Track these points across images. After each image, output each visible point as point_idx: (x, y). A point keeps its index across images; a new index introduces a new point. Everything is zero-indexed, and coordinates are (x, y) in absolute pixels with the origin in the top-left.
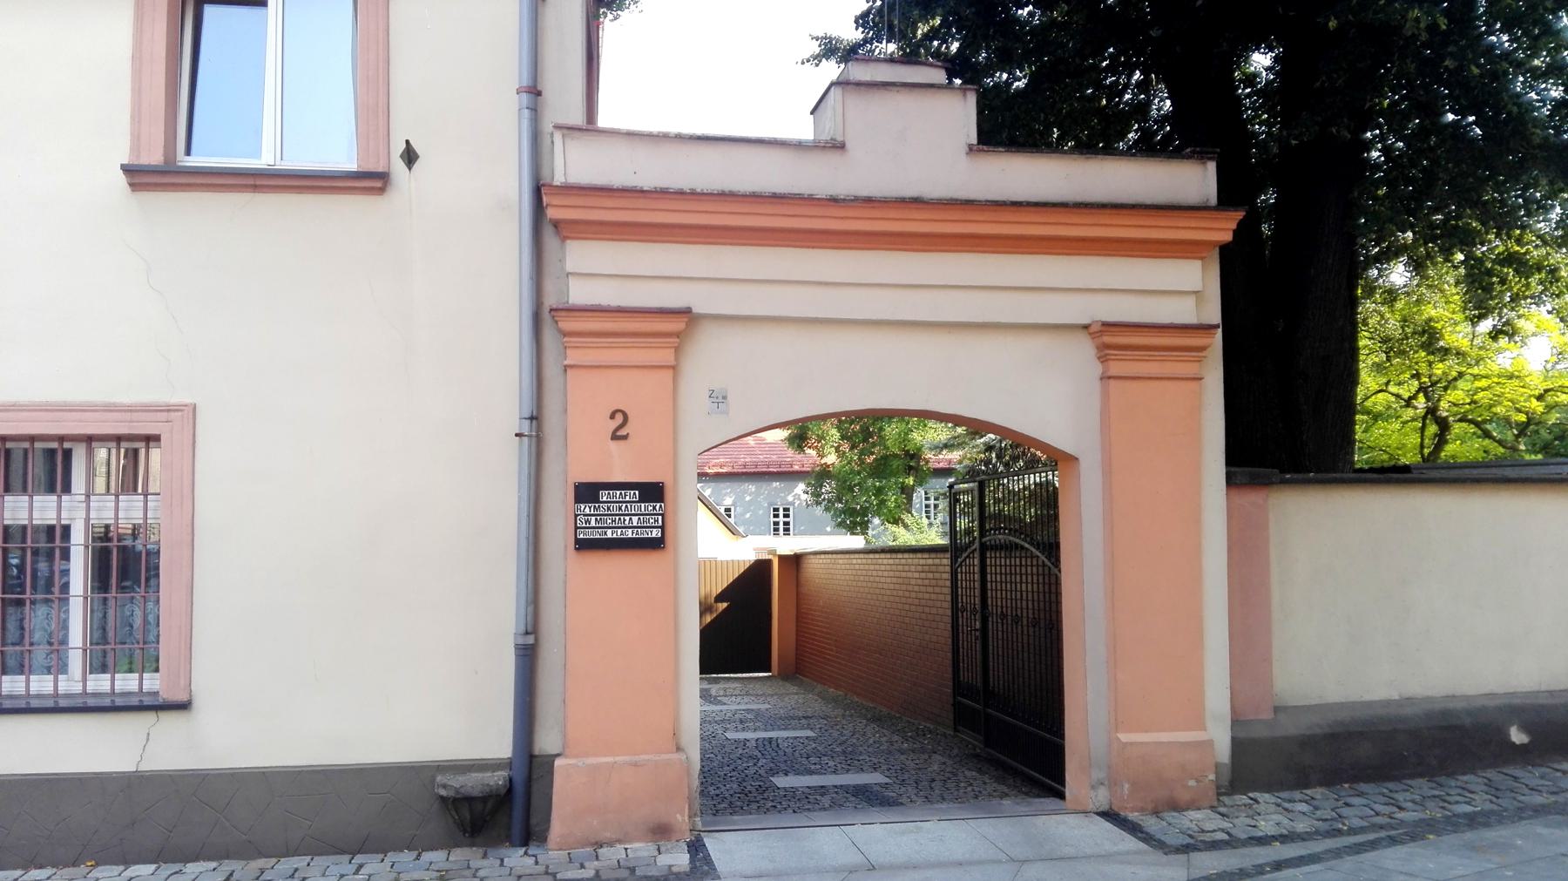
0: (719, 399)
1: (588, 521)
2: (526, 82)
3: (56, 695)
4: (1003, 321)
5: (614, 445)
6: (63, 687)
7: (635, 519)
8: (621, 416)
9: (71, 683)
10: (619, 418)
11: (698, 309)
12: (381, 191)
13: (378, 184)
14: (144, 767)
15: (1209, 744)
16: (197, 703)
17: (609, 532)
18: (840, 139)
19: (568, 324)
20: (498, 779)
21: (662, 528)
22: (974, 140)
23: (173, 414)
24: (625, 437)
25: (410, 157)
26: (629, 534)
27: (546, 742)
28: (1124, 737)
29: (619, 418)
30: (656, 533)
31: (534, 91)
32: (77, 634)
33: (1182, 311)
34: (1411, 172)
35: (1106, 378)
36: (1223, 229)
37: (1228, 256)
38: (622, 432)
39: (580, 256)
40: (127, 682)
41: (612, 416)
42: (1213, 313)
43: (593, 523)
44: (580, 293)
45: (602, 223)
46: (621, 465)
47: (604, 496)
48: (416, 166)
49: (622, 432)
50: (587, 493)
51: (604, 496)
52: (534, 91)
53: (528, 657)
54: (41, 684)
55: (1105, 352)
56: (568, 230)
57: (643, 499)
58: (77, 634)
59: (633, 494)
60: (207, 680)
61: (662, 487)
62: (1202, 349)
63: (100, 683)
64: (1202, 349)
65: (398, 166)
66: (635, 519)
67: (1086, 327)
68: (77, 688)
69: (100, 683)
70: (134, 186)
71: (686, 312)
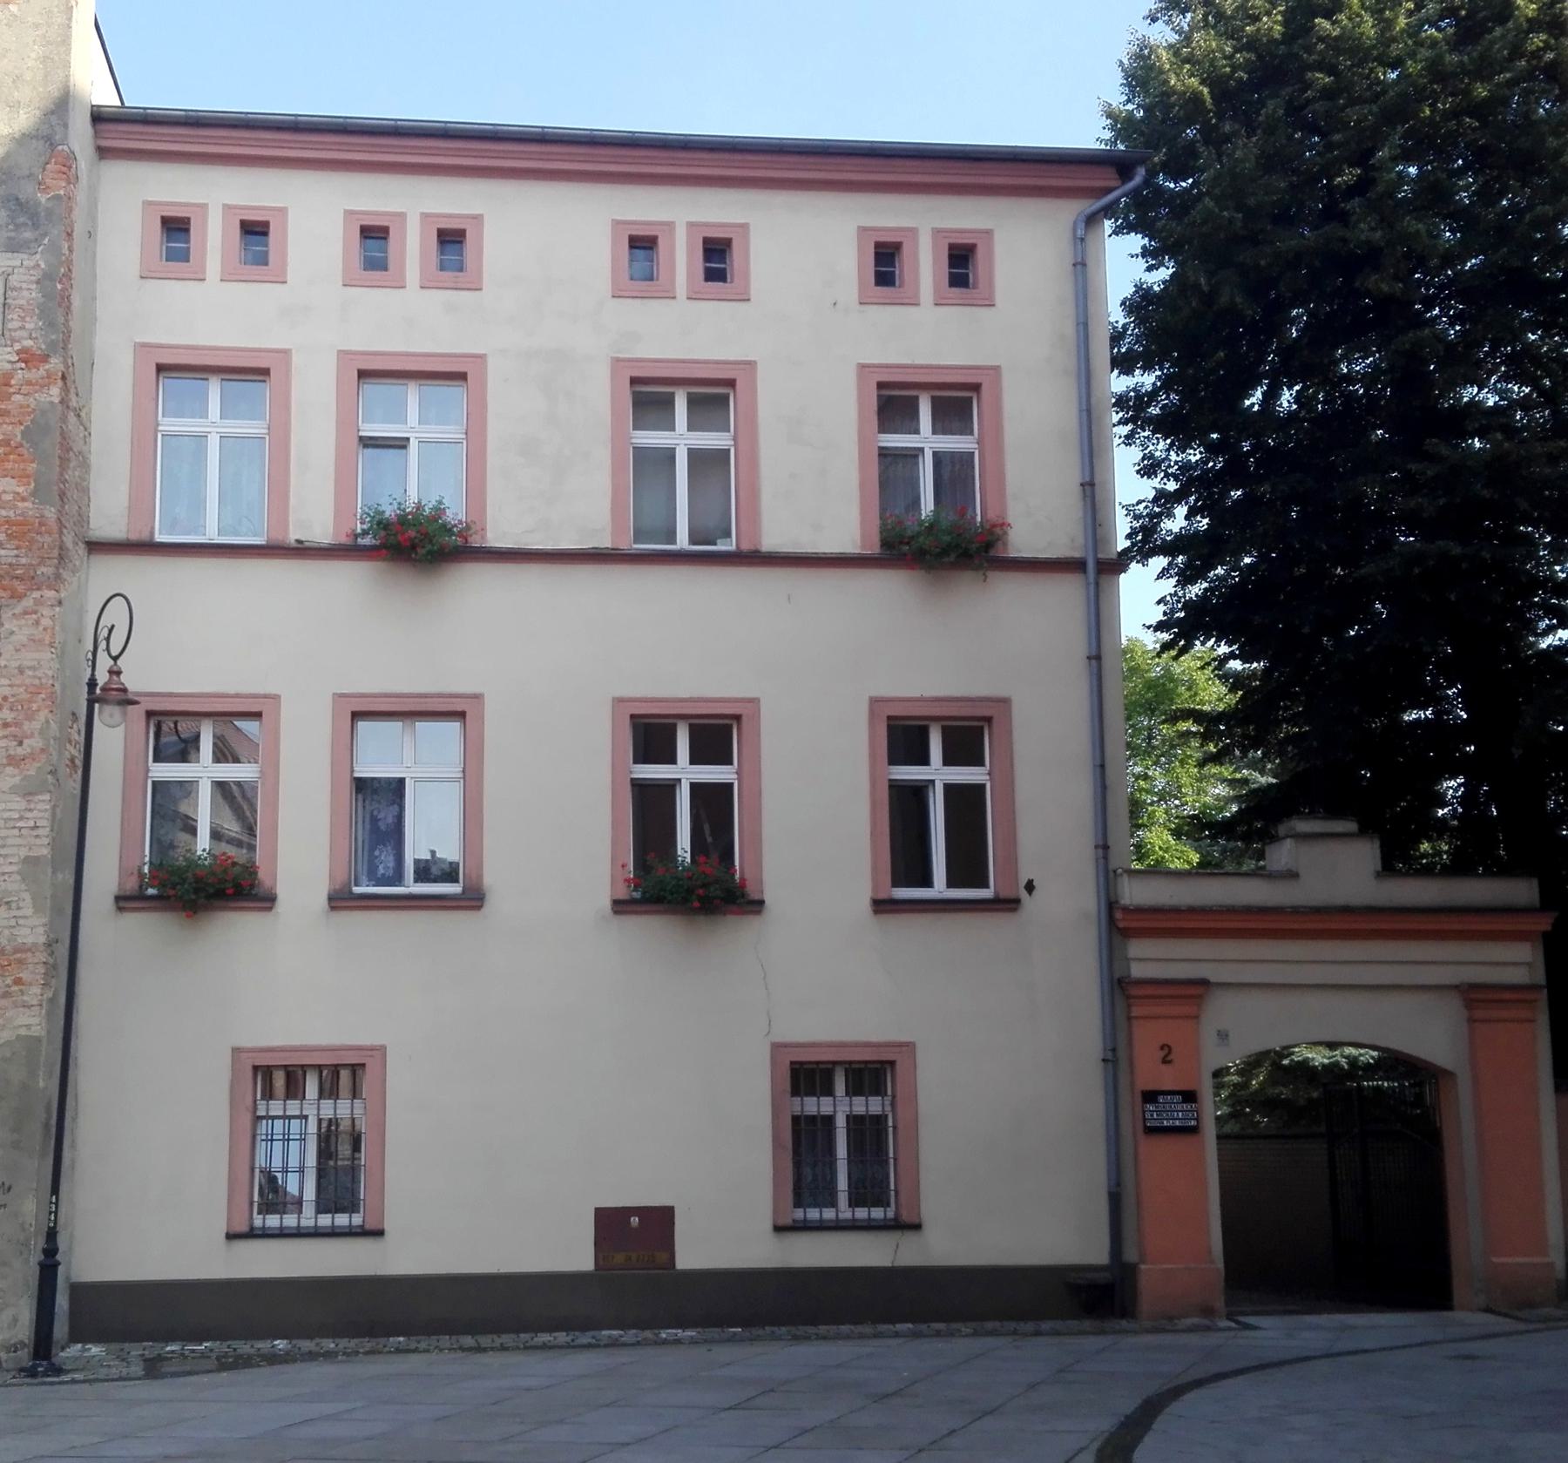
0: (1223, 1036)
1: (1152, 1115)
3: (333, 1226)
5: (1164, 1067)
6: (304, 1223)
7: (1180, 1114)
8: (1166, 1048)
10: (1166, 1050)
11: (1212, 980)
12: (1014, 910)
13: (268, 905)
15: (1551, 1265)
18: (1294, 869)
19: (1134, 991)
21: (1197, 1119)
22: (1380, 869)
23: (904, 1049)
24: (1170, 1062)
25: (1030, 887)
26: (1177, 1123)
27: (1130, 1255)
28: (1495, 1260)
30: (1193, 1123)
31: (1105, 847)
33: (1517, 976)
35: (1471, 1021)
36: (1544, 923)
37: (1546, 937)
38: (1169, 1058)
39: (1138, 948)
41: (1162, 1048)
42: (1540, 977)
43: (1155, 1116)
44: (1137, 971)
45: (1292, 930)
46: (1168, 1080)
48: (1034, 893)
49: (1169, 1058)
50: (1150, 1097)
52: (1105, 847)
54: (829, 1214)
55: (1470, 1004)
56: (1128, 933)
59: (1178, 1098)
62: (1535, 1001)
63: (325, 1220)
64: (1535, 1001)
65: (1023, 894)
66: (1180, 1114)
67: (1456, 987)
68: (311, 1223)
69: (325, 1220)
70: (876, 912)
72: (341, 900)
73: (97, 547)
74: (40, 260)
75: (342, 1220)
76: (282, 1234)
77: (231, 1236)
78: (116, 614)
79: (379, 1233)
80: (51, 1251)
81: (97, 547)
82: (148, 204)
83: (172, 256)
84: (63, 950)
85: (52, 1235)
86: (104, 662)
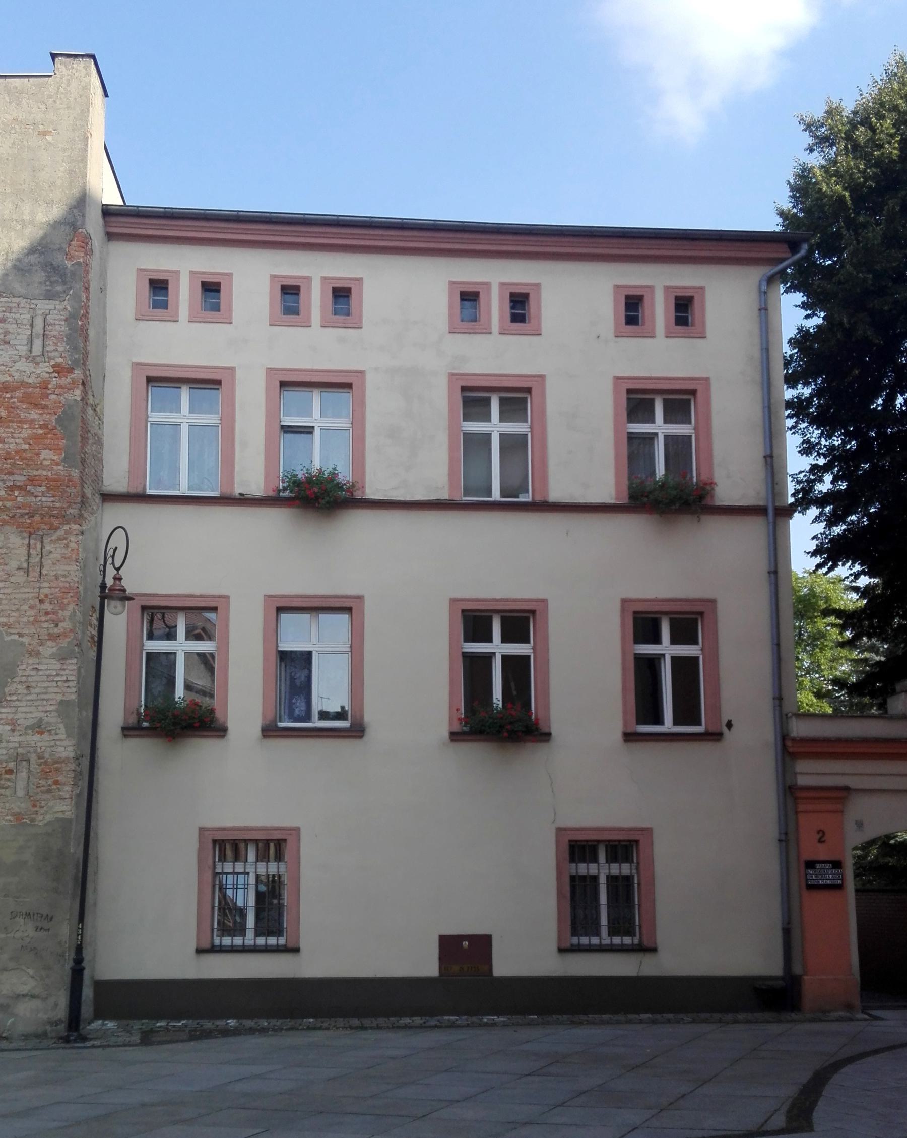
1: (812, 877)
2: (777, 695)
4: (236, 424)
5: (819, 845)
7: (831, 876)
8: (821, 832)
9: (250, 939)
10: (821, 834)
12: (719, 740)
14: (640, 974)
16: (659, 948)
17: (821, 882)
20: (781, 983)
21: (842, 880)
24: (824, 841)
25: (729, 725)
26: (829, 882)
29: (821, 833)
30: (839, 882)
32: (604, 920)
34: (869, 173)
38: (823, 839)
40: (272, 941)
41: (818, 832)
43: (814, 877)
44: (802, 781)
46: (822, 853)
47: (818, 866)
49: (823, 839)
50: (810, 865)
51: (818, 866)
53: (787, 932)
56: (795, 756)
57: (834, 867)
58: (604, 920)
59: (829, 866)
60: (661, 939)
61: (652, 830)
63: (261, 941)
65: (725, 729)
66: (831, 876)
68: (252, 943)
69: (261, 941)
71: (847, 789)
72: (270, 731)
73: (109, 497)
74: (67, 305)
75: (272, 941)
76: (233, 950)
77: (199, 951)
78: (118, 539)
79: (296, 950)
80: (79, 960)
81: (109, 497)
82: (140, 270)
83: (157, 305)
84: (86, 762)
85: (79, 949)
86: (111, 572)
